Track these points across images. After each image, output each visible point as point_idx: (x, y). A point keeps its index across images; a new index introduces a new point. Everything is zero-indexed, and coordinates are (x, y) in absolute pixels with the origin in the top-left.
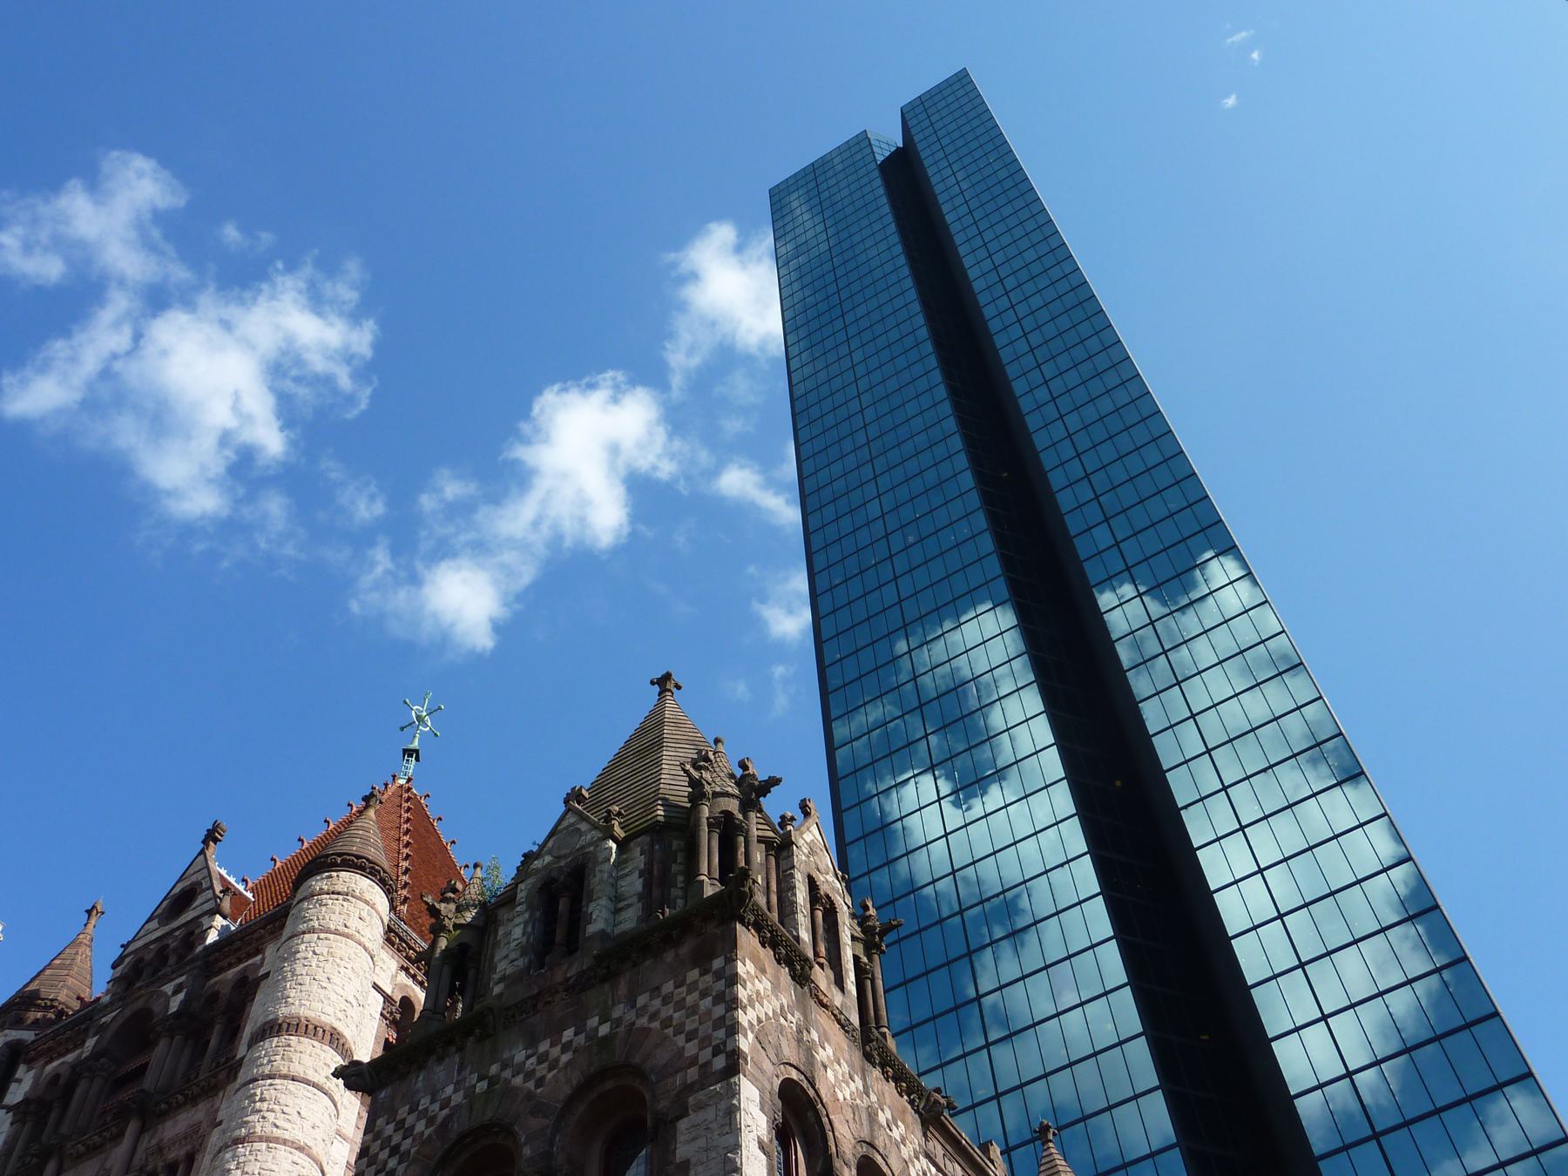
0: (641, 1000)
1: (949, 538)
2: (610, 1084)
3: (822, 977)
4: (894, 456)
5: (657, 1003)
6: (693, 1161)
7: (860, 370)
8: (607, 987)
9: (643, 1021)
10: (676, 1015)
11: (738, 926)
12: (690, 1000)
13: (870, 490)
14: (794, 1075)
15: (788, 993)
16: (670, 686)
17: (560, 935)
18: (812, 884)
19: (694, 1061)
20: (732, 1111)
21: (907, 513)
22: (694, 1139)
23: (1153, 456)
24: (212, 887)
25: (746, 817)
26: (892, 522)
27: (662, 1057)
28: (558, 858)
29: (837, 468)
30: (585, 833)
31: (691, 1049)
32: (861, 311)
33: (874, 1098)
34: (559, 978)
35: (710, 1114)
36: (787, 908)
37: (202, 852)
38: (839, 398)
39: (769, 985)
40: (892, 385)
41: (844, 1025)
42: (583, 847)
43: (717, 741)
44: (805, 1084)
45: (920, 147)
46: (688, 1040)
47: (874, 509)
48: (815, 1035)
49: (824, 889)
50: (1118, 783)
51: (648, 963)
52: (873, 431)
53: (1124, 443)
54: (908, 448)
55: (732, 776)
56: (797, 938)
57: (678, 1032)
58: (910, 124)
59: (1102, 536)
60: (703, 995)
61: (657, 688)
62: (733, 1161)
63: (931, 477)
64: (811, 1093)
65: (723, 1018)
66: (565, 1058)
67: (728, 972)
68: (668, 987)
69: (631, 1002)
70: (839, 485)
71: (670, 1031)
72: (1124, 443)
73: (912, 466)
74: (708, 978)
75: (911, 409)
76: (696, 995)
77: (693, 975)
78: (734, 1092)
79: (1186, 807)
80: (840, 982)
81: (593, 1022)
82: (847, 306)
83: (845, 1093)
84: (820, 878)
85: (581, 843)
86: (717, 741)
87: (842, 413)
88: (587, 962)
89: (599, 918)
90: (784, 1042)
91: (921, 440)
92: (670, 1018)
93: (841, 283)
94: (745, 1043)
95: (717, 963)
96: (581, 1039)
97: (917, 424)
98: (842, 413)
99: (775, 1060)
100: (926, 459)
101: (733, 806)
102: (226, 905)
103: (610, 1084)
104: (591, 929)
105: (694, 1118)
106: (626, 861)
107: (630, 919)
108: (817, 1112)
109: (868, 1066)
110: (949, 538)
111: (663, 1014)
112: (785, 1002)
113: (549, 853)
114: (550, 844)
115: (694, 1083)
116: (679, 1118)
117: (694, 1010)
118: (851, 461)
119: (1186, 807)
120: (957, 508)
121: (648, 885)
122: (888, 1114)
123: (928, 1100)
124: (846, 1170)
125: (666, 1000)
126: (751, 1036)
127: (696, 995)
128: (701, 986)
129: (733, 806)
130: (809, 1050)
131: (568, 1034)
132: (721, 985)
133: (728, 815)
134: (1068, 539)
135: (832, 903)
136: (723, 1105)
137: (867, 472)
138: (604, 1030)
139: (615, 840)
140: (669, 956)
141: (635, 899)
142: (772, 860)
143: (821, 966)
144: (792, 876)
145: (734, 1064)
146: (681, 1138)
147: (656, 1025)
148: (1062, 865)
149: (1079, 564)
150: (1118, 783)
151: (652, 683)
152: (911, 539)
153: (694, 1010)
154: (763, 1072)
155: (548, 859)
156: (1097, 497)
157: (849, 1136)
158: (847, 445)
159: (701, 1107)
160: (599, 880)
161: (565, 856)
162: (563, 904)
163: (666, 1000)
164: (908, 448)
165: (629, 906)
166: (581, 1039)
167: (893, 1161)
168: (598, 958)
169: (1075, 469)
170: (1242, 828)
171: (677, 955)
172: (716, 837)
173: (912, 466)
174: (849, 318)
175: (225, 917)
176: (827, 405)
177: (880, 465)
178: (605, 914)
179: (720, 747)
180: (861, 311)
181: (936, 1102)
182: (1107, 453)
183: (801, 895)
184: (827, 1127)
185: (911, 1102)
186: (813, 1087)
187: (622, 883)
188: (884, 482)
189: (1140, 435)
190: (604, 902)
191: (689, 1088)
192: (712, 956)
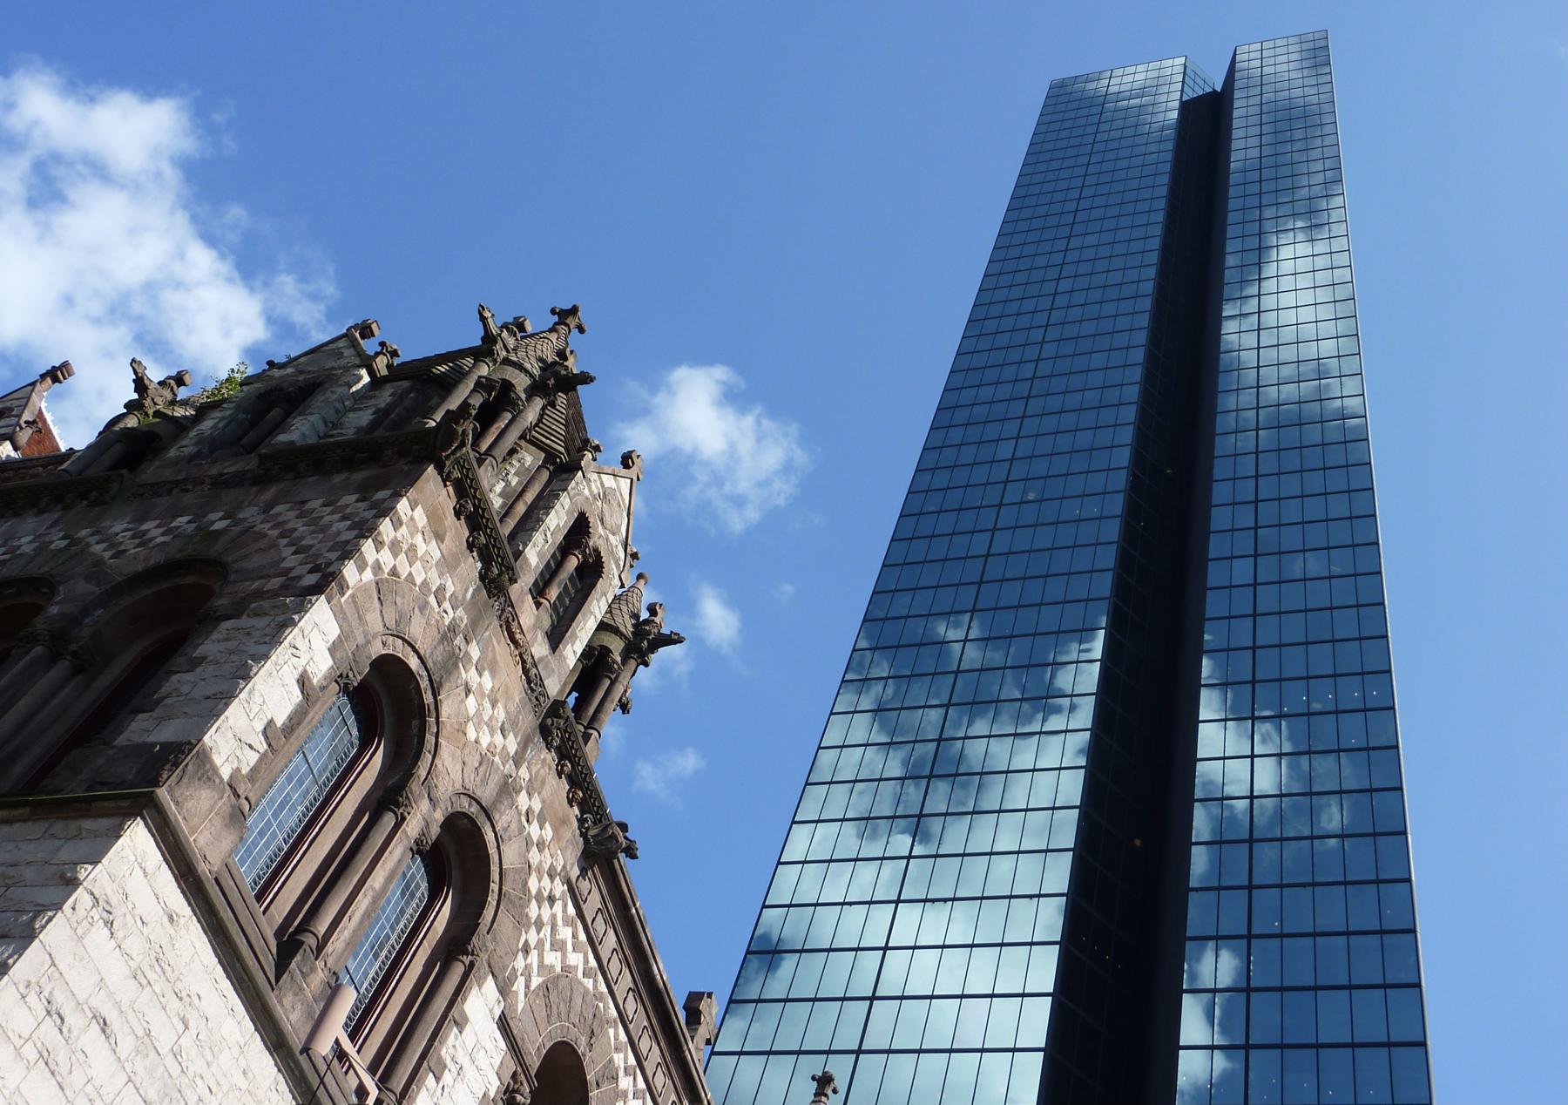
1: (1072, 510)
2: (190, 580)
3: (530, 616)
4: (1055, 403)
7: (1061, 300)
11: (431, 469)
13: (1011, 428)
14: (414, 663)
16: (572, 322)
21: (1039, 467)
23: (1339, 506)
24: (19, 416)
25: (529, 399)
26: (1019, 470)
27: (257, 561)
28: (301, 372)
29: (986, 393)
32: (1091, 240)
33: (524, 773)
34: (214, 471)
35: (261, 623)
37: (33, 384)
38: (1024, 321)
40: (1089, 328)
41: (532, 682)
42: (333, 368)
44: (424, 684)
45: (1237, 94)
47: (1006, 450)
48: (474, 651)
52: (1045, 368)
53: (1315, 482)
54: (1074, 401)
55: (541, 360)
58: (1238, 58)
59: (1242, 571)
62: (248, 668)
63: (1084, 439)
64: (428, 698)
69: (267, 508)
70: (980, 411)
72: (1315, 482)
73: (1068, 421)
74: (362, 505)
75: (1098, 360)
80: (556, 638)
82: (1077, 229)
87: (1019, 338)
91: (1092, 397)
93: (1083, 204)
95: (380, 495)
97: (1096, 379)
98: (1019, 338)
99: (392, 625)
100: (1088, 418)
101: (521, 382)
102: (24, 436)
103: (190, 580)
105: (244, 622)
106: (371, 398)
109: (538, 739)
110: (1072, 510)
114: (302, 360)
116: (228, 617)
118: (1004, 391)
119: (1196, 890)
120: (1097, 482)
122: (537, 806)
123: (605, 829)
124: (425, 805)
129: (521, 382)
130: (454, 661)
133: (507, 386)
134: (1204, 560)
137: (1017, 408)
139: (371, 373)
140: (338, 479)
142: (545, 475)
144: (557, 497)
145: (325, 580)
147: (275, 533)
148: (1031, 897)
149: (1204, 589)
150: (1138, 842)
151: (553, 312)
152: (1031, 496)
156: (1256, 528)
158: (1009, 373)
159: (258, 614)
164: (1074, 401)
169: (1246, 490)
170: (1249, 937)
173: (1068, 421)
174: (1074, 243)
175: (16, 449)
176: (1007, 323)
177: (1034, 406)
180: (1091, 240)
181: (614, 837)
182: (1291, 485)
185: (581, 821)
186: (435, 696)
187: (351, 415)
188: (1030, 426)
189: (1337, 481)
191: (260, 594)
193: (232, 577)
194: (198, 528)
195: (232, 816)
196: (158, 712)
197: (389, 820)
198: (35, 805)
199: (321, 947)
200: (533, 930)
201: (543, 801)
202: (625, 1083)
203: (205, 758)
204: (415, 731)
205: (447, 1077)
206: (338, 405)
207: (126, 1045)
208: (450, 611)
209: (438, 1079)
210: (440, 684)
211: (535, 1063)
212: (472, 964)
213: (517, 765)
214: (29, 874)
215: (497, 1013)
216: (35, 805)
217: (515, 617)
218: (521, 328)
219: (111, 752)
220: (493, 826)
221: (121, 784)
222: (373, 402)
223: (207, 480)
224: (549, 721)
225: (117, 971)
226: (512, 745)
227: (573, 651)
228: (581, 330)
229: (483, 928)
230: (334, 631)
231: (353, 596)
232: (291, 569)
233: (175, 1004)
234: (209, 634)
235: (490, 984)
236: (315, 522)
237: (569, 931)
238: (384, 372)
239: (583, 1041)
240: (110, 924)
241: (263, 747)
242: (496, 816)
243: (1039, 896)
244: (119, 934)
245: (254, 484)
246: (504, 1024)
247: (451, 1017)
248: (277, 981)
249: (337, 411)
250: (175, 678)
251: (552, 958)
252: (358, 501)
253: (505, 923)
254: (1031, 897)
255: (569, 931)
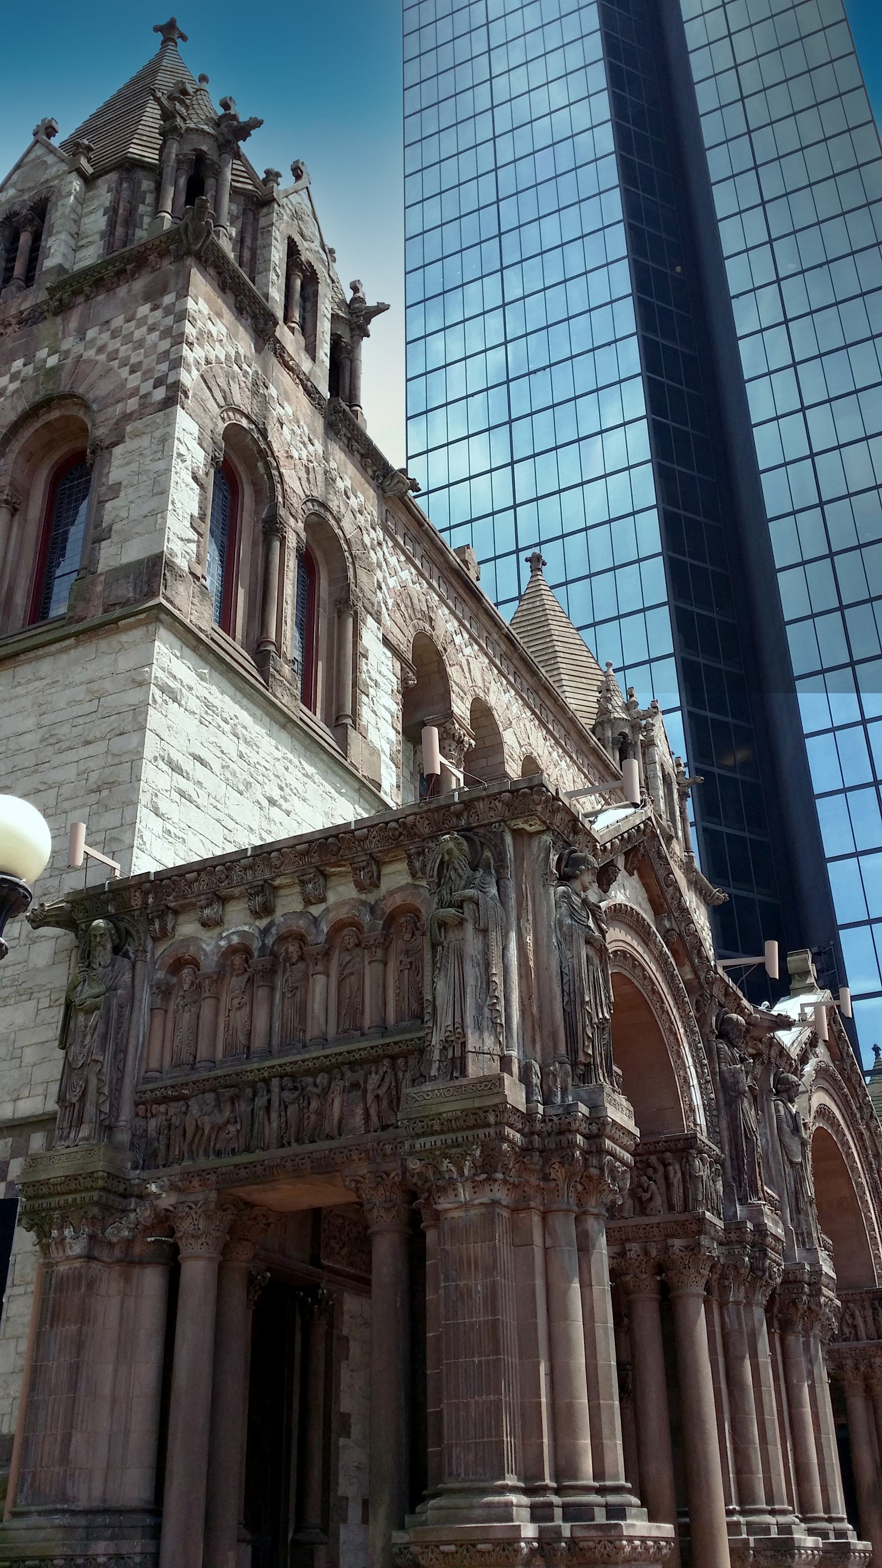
0: (91, 334)
2: (55, 414)
3: (290, 339)
5: (106, 336)
6: (124, 483)
8: (59, 319)
9: (90, 353)
10: (123, 348)
12: (137, 335)
14: (244, 423)
15: (245, 345)
17: (19, 269)
18: (292, 250)
19: (135, 392)
20: (166, 441)
22: (127, 464)
27: (104, 388)
28: (22, 191)
30: (52, 166)
31: (134, 381)
35: (145, 441)
36: (255, 260)
39: (224, 331)
41: (311, 392)
42: (47, 181)
43: (203, 78)
46: (132, 372)
48: (273, 391)
49: (306, 256)
50: (678, 269)
51: (101, 297)
56: (267, 296)
57: (123, 365)
60: (151, 330)
61: (160, 36)
64: (337, 531)
65: (167, 352)
66: (13, 387)
67: (178, 308)
68: (118, 322)
69: (81, 334)
71: (115, 364)
74: (159, 313)
76: (144, 329)
77: (144, 310)
78: (171, 423)
79: (737, 296)
80: (311, 350)
81: (43, 353)
83: (300, 453)
84: (302, 245)
85: (47, 176)
86: (203, 78)
88: (43, 296)
89: (57, 252)
90: (235, 387)
92: (117, 351)
94: (189, 378)
95: (168, 299)
96: (30, 369)
103: (55, 414)
104: (49, 263)
107: (90, 256)
108: (268, 466)
111: (111, 348)
112: (242, 351)
113: (14, 185)
114: (15, 177)
115: (131, 414)
117: (140, 344)
119: (737, 296)
121: (112, 225)
122: (348, 483)
124: (292, 521)
125: (114, 335)
126: (195, 373)
127: (144, 329)
128: (150, 321)
131: (18, 364)
132: (169, 320)
133: (200, 156)
135: (314, 273)
136: (158, 434)
138: (52, 361)
140: (122, 291)
141: (97, 237)
143: (292, 330)
146: (115, 462)
147: (102, 357)
148: (609, 344)
150: (678, 269)
153: (140, 344)
154: (205, 410)
155: (11, 192)
157: (299, 491)
159: (137, 435)
160: (60, 215)
161: (30, 189)
162: (25, 239)
163: (114, 335)
165: (91, 243)
166: (30, 369)
167: (347, 523)
168: (51, 290)
171: (130, 291)
172: (689, 803)
178: (63, 249)
179: (204, 85)
183: (278, 255)
184: (277, 479)
190: (63, 236)
191: (127, 417)
192: (164, 291)
193: (95, 407)
194: (36, 369)
195: (202, 593)
196: (115, 538)
197: (277, 544)
198: (76, 635)
199: (278, 649)
200: (378, 572)
201: (351, 478)
202: (458, 639)
203: (170, 565)
204: (262, 470)
205: (372, 692)
206: (73, 216)
207: (216, 765)
208: (248, 369)
209: (367, 696)
210: (266, 429)
211: (409, 656)
212: (356, 613)
213: (327, 460)
214: (108, 685)
215: (381, 637)
216: (76, 635)
217: (283, 348)
218: (184, 92)
219: (102, 578)
220: (331, 513)
221: (126, 603)
222: (95, 204)
223: (13, 321)
224: (333, 418)
225: (189, 724)
226: (319, 447)
227: (324, 350)
228: (184, 38)
229: (353, 586)
230: (194, 429)
231: (194, 395)
232: (137, 389)
233: (228, 728)
234: (109, 461)
235: (370, 621)
236: (128, 339)
237: (394, 558)
238: (90, 170)
239: (428, 627)
240: (175, 700)
241: (195, 537)
242: (330, 504)
243: (616, 341)
244: (183, 702)
245: (55, 314)
246: (386, 642)
247: (359, 655)
248: (267, 683)
249: (75, 221)
250: (108, 505)
251: (392, 582)
252: (152, 310)
253: (362, 574)
254: (609, 344)
255: (394, 558)
